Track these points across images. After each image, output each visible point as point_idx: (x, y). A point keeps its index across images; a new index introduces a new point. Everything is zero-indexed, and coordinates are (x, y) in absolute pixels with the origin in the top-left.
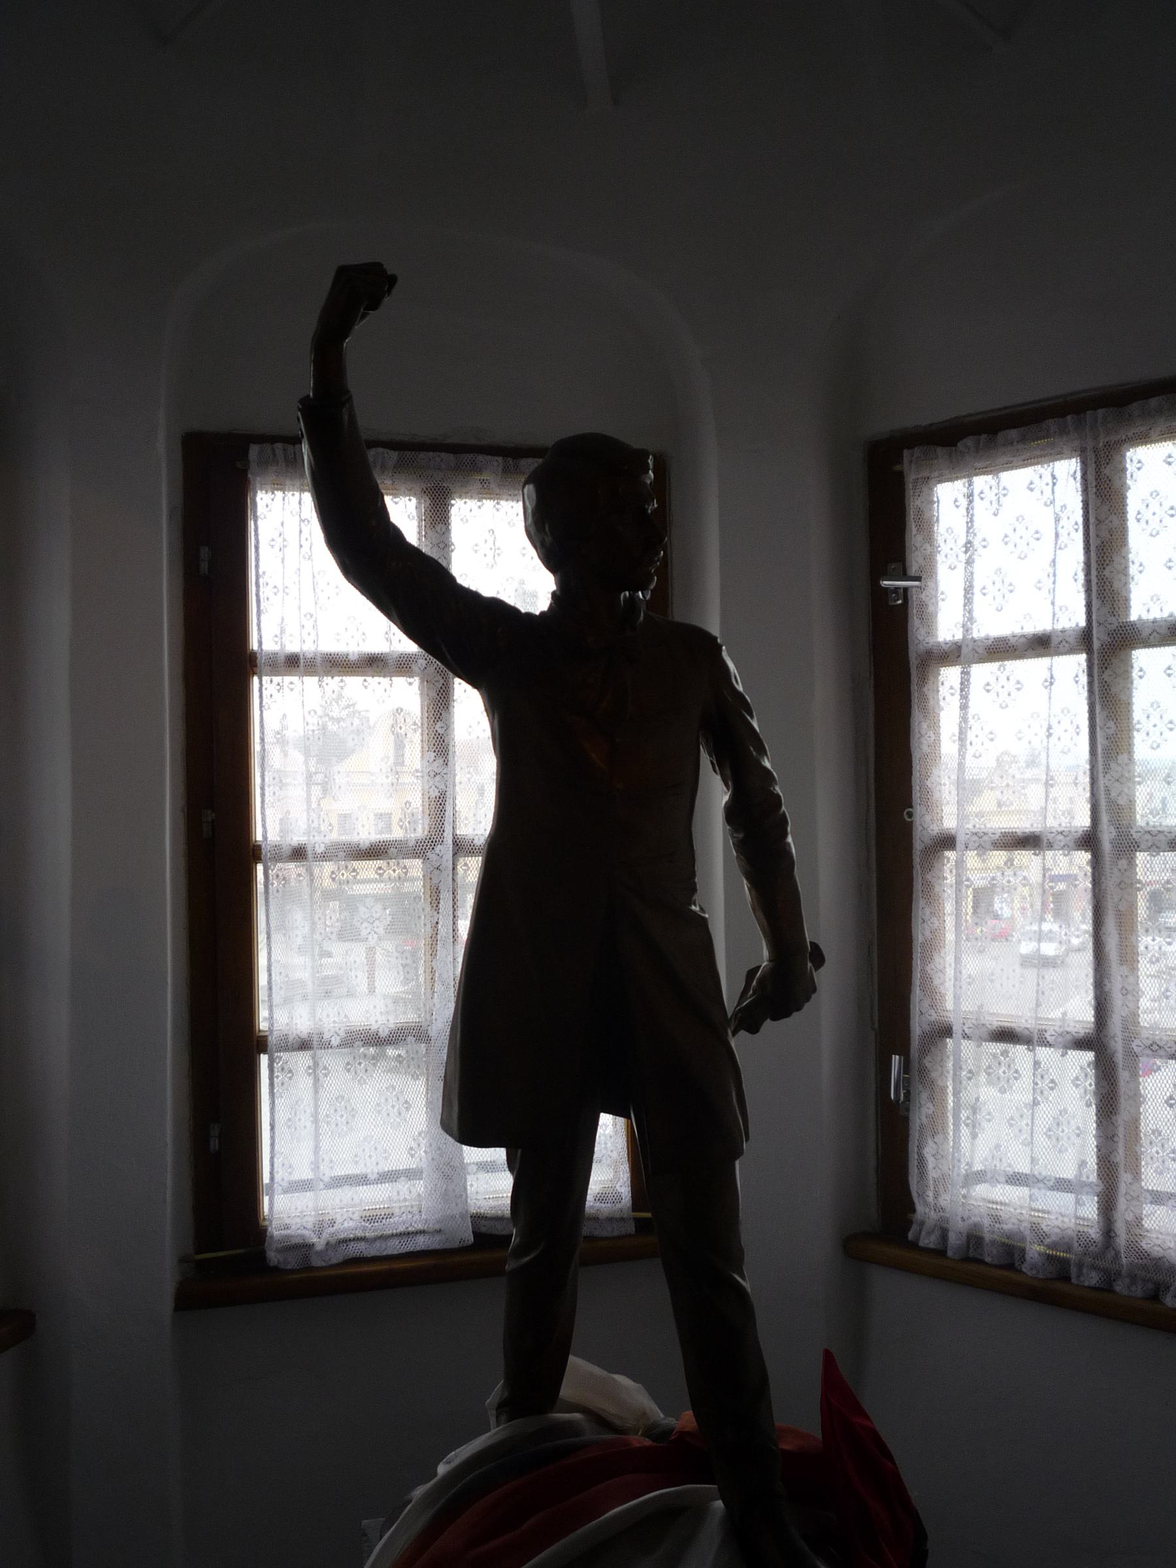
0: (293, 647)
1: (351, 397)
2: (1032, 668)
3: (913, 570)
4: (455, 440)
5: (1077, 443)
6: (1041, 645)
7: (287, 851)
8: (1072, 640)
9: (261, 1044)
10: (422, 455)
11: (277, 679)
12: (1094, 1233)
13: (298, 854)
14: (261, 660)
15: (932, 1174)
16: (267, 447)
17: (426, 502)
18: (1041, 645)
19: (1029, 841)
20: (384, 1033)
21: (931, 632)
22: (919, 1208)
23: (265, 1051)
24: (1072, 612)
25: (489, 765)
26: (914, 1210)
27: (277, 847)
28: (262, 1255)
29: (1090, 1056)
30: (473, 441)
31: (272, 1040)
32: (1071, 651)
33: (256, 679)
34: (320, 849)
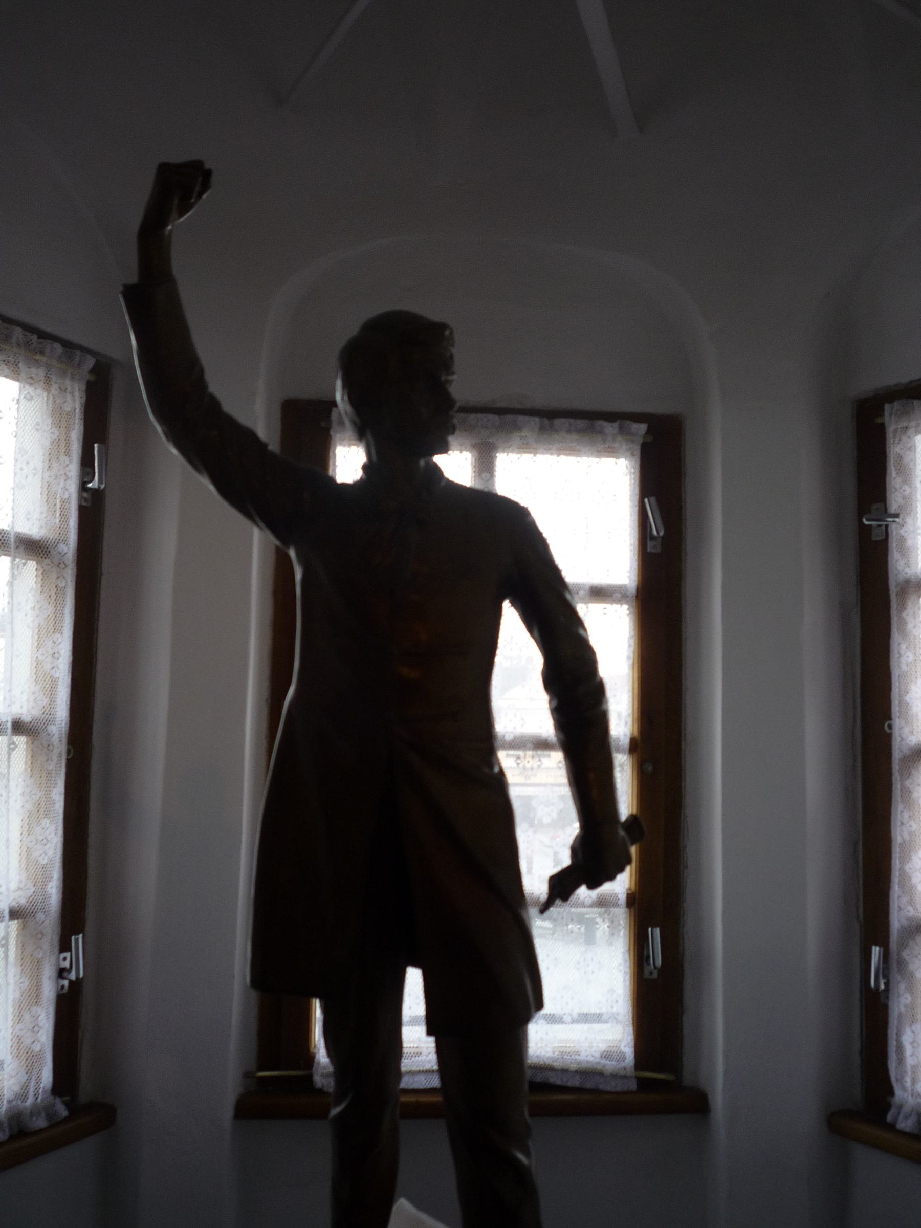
10: (473, 416)
22: (898, 1092)
26: (891, 1093)
28: (309, 1078)
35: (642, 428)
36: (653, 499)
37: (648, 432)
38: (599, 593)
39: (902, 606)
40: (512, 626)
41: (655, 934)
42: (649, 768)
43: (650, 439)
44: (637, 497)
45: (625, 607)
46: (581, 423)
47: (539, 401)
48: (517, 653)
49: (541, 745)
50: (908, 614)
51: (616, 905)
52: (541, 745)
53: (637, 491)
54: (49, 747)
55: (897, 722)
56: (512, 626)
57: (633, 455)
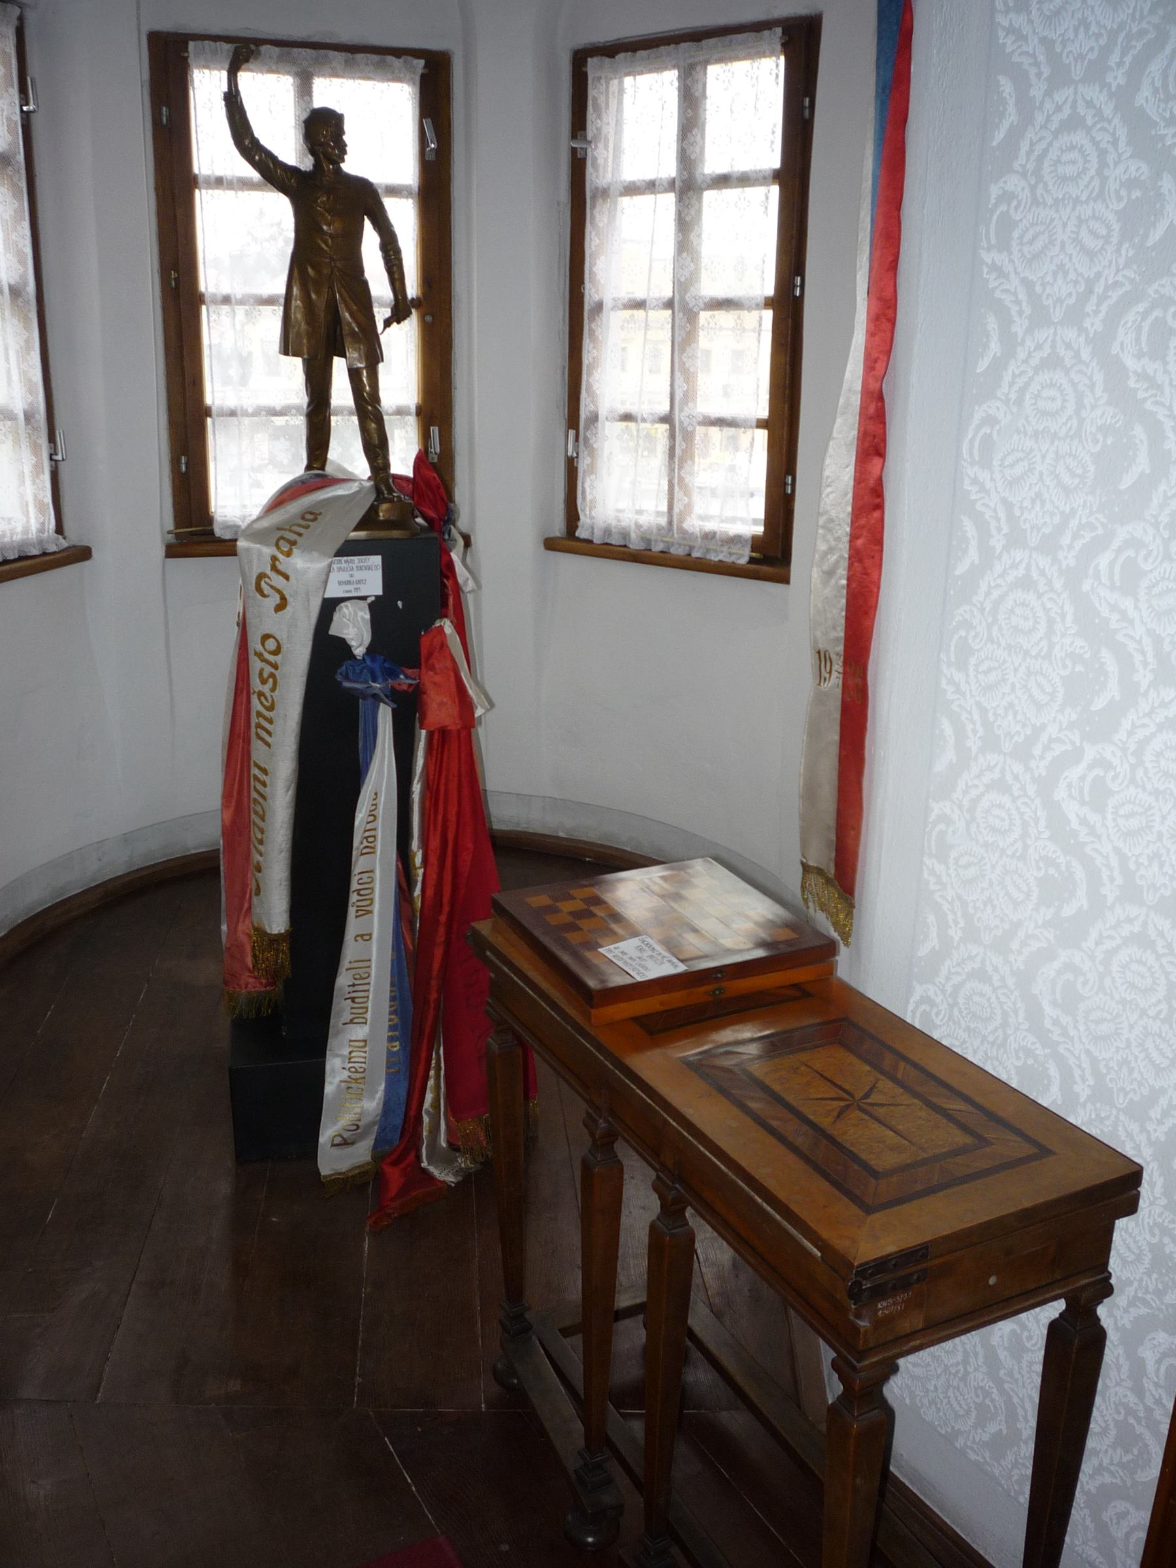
0: (219, 173)
1: (388, 1068)
2: (647, 200)
3: (589, 138)
4: (316, 39)
5: (674, 62)
6: (651, 187)
7: (219, 298)
8: (665, 184)
9: (208, 412)
10: (295, 50)
11: (210, 191)
12: (663, 521)
13: (226, 300)
14: (200, 180)
15: (589, 497)
16: (199, 43)
17: (298, 81)
18: (651, 187)
19: (640, 305)
20: (278, 408)
21: (703, 169)
22: (582, 517)
23: (210, 416)
24: (669, 169)
25: (368, 275)
26: (578, 519)
27: (214, 295)
28: (212, 533)
29: (667, 426)
30: (328, 41)
31: (214, 411)
32: (666, 191)
33: (197, 191)
34: (239, 296)
35: (421, 63)
36: (429, 120)
37: (425, 66)
38: (393, 191)
39: (593, 206)
40: (368, 224)
41: (435, 431)
42: (429, 319)
43: (426, 71)
44: (417, 118)
45: (411, 201)
46: (375, 58)
47: (345, 38)
48: (370, 240)
49: (691, 102)
50: (596, 212)
51: (409, 414)
52: (691, 102)
53: (417, 113)
54: (27, 302)
55: (587, 284)
56: (368, 224)
57: (414, 83)
